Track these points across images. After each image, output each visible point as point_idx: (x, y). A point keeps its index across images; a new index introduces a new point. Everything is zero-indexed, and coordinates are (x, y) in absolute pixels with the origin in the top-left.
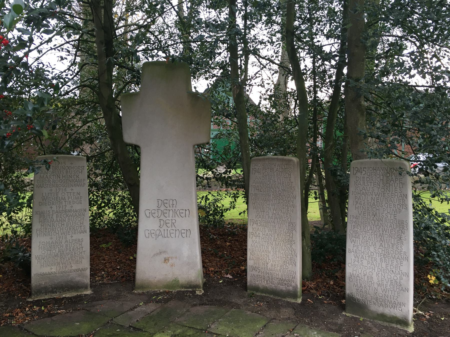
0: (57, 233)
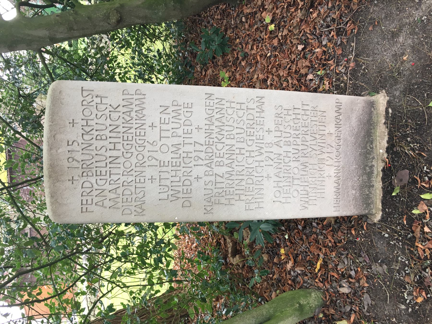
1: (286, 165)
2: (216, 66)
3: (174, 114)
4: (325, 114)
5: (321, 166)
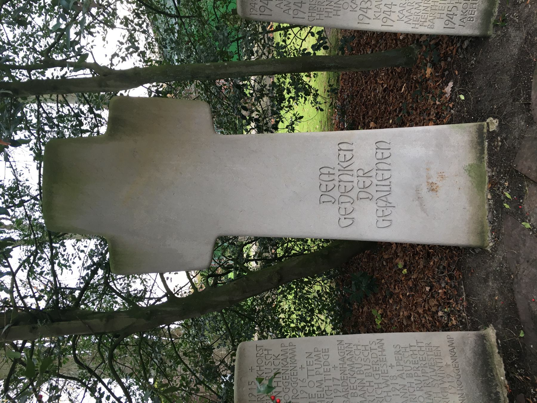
0: (385, 394)
1: (411, 394)
2: (369, 303)
3: (316, 358)
4: (439, 349)
5: (445, 394)
